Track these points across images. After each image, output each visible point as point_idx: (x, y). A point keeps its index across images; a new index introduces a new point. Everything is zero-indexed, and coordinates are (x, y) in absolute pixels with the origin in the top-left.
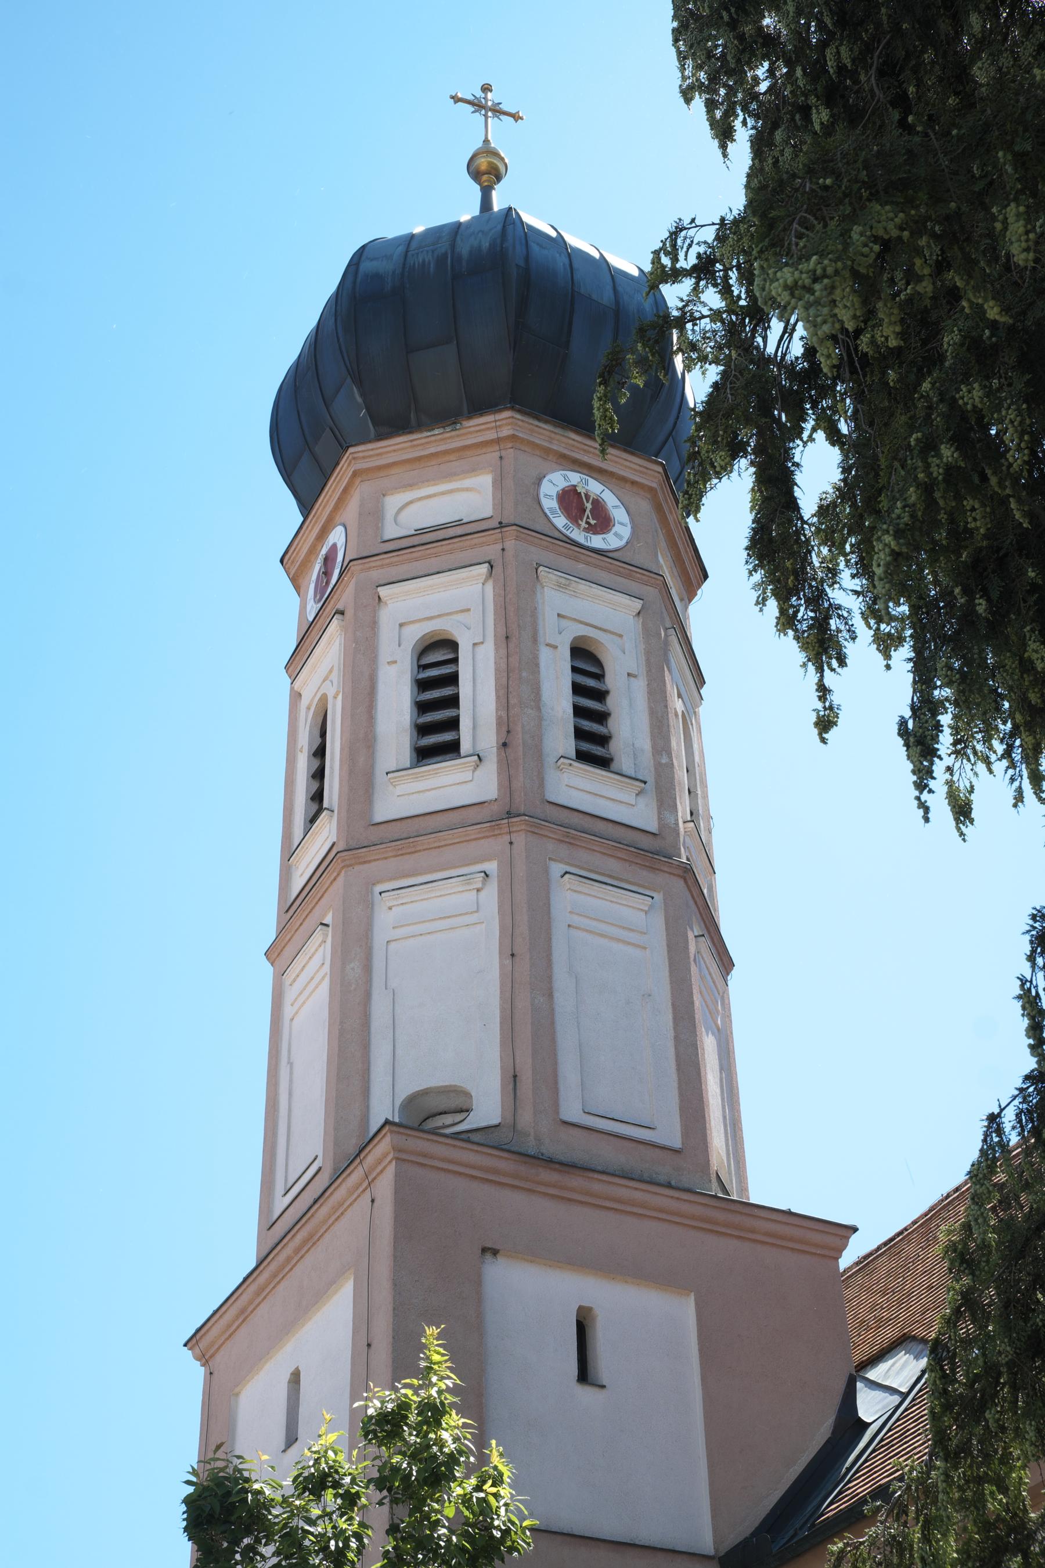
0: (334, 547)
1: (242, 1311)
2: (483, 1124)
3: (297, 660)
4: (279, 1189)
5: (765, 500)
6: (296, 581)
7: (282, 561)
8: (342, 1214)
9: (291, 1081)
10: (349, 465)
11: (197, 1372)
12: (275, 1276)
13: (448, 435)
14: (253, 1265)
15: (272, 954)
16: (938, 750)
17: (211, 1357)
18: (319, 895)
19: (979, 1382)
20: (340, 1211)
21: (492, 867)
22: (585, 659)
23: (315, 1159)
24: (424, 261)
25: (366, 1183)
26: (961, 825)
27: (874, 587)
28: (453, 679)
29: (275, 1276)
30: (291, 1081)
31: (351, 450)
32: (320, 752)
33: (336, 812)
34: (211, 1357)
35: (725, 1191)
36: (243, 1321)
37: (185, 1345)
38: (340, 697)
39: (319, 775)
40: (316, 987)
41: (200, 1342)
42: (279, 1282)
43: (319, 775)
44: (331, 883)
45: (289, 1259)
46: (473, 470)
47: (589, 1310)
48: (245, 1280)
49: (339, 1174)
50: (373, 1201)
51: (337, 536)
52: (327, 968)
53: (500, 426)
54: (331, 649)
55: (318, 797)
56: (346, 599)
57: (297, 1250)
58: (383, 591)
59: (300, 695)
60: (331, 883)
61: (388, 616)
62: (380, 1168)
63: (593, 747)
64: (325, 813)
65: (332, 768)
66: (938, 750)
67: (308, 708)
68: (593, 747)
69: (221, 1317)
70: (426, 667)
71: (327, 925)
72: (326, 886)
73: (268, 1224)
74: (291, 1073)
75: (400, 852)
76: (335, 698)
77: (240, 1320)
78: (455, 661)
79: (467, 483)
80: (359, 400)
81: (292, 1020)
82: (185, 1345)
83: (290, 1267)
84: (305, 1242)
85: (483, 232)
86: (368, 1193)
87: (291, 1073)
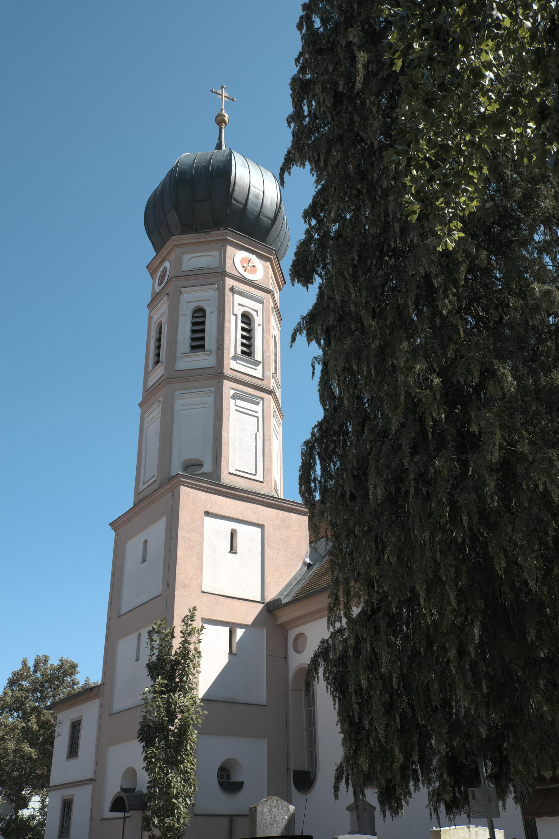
0: (165, 268)
1: (129, 518)
2: (206, 472)
3: (152, 305)
4: (142, 482)
5: (311, 523)
6: (152, 274)
11: (113, 533)
12: (140, 510)
21: (213, 389)
22: (247, 318)
28: (203, 323)
29: (140, 510)
31: (174, 237)
32: (159, 340)
43: (158, 347)
45: (145, 506)
46: (214, 250)
48: (130, 509)
49: (161, 485)
51: (167, 264)
52: (159, 415)
54: (163, 307)
55: (158, 355)
56: (170, 289)
57: (148, 504)
58: (182, 290)
59: (152, 318)
63: (198, 343)
66: (498, 816)
67: (155, 323)
68: (198, 343)
70: (195, 317)
73: (137, 493)
78: (204, 316)
79: (211, 253)
80: (177, 217)
84: (150, 502)
86: (171, 493)
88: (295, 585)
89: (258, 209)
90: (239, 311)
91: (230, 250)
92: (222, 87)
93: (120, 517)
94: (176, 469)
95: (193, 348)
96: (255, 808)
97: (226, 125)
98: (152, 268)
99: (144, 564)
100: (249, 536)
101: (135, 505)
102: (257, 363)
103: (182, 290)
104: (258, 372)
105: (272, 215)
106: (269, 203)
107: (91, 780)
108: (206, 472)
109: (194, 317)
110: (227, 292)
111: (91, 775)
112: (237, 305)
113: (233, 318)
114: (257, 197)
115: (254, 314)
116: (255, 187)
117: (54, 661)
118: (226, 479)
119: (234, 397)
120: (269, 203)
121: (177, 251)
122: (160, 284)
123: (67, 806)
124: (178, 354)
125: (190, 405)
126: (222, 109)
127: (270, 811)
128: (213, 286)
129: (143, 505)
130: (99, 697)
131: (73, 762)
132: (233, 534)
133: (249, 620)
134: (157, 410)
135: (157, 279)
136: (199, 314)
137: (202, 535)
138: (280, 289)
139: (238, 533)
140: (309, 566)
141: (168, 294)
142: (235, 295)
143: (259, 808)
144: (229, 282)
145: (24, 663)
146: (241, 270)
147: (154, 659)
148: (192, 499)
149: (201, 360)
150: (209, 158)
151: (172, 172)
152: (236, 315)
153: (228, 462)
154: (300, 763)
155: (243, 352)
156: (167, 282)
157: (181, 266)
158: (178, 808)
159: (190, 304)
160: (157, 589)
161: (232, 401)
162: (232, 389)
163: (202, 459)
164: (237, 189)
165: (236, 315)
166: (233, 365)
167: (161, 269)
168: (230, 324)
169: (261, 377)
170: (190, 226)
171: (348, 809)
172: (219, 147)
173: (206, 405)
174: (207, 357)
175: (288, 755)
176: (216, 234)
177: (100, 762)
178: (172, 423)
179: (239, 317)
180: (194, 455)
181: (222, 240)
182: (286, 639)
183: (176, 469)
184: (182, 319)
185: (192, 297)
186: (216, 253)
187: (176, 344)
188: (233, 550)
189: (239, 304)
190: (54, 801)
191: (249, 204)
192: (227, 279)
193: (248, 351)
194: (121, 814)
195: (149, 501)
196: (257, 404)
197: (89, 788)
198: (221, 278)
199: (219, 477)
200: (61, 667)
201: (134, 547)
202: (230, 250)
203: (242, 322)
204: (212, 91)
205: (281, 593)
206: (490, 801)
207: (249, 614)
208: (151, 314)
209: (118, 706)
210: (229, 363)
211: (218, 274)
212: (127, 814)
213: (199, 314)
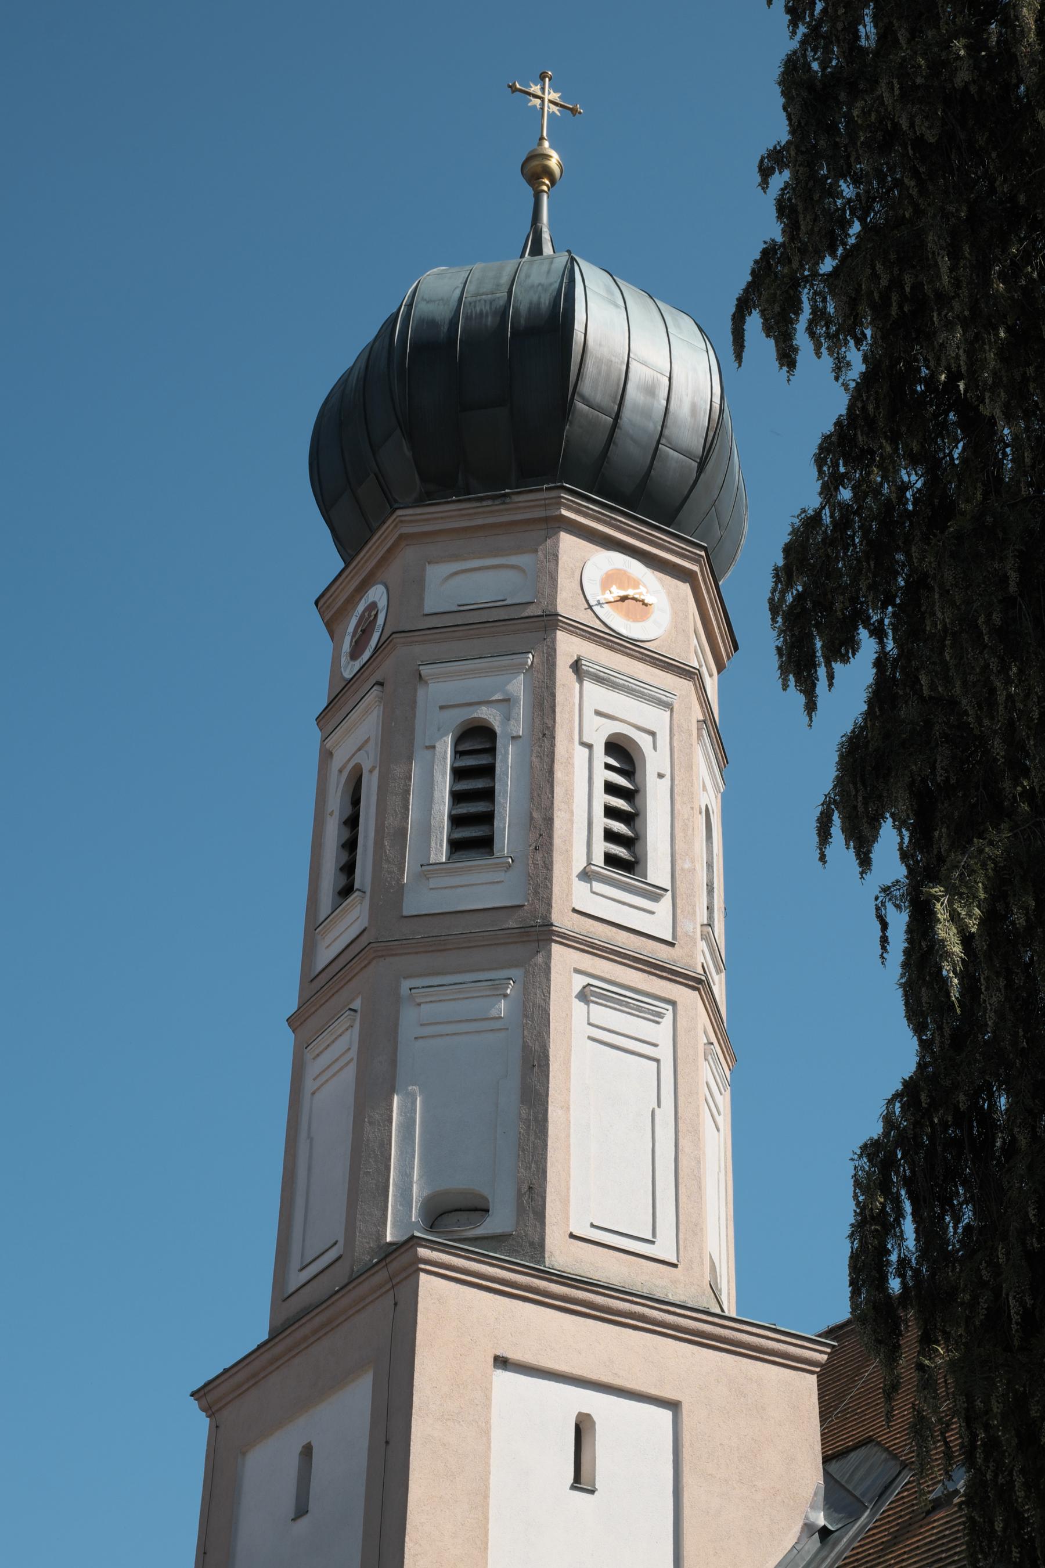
0: (373, 606)
4: (295, 1263)
6: (331, 625)
7: (317, 603)
8: (363, 1308)
9: (310, 1157)
10: (396, 526)
11: (202, 1423)
13: (496, 508)
14: (266, 1337)
15: (295, 1022)
17: (218, 1411)
18: (348, 978)
20: (362, 1304)
22: (622, 753)
23: (335, 1243)
24: (481, 311)
25: (389, 1285)
30: (310, 1157)
31: (399, 512)
32: (352, 822)
33: (368, 894)
34: (218, 1411)
35: (723, 1310)
36: (253, 1385)
37: (192, 1395)
38: (376, 772)
39: (350, 845)
40: (341, 1069)
41: (205, 1395)
42: (294, 1356)
43: (350, 845)
44: (362, 969)
45: (305, 1338)
47: (588, 1416)
48: (259, 1347)
50: (396, 1304)
51: (377, 594)
52: (353, 1053)
53: (549, 504)
54: (366, 723)
55: (349, 869)
56: (385, 669)
57: (315, 1332)
59: (331, 754)
60: (362, 969)
62: (404, 1275)
63: (473, 831)
64: (357, 894)
65: (365, 846)
67: (340, 771)
68: (473, 831)
69: (230, 1377)
71: (355, 1011)
72: (356, 971)
73: (281, 1296)
74: (311, 1148)
75: (431, 949)
76: (371, 771)
77: (251, 1383)
78: (492, 750)
79: (513, 560)
80: (408, 454)
81: (313, 1094)
82: (192, 1395)
83: (305, 1345)
85: (542, 285)
87: (311, 1148)
90: (599, 733)
92: (543, 77)
93: (226, 1371)
100: (631, 1436)
101: (275, 1334)
102: (654, 894)
103: (425, 670)
104: (658, 919)
105: (696, 444)
108: (493, 1219)
110: (563, 673)
112: (588, 714)
115: (644, 741)
118: (560, 1253)
121: (409, 554)
122: (354, 655)
125: (442, 1016)
128: (517, 659)
132: (583, 1430)
135: (347, 640)
136: (477, 743)
137: (485, 1432)
138: (720, 667)
141: (381, 684)
142: (587, 684)
148: (454, 1316)
149: (481, 887)
152: (590, 747)
153: (566, 1202)
155: (611, 860)
156: (376, 650)
161: (579, 1007)
162: (577, 971)
163: (485, 1192)
165: (590, 747)
166: (579, 895)
167: (361, 607)
168: (570, 773)
176: (526, 503)
179: (600, 749)
181: (546, 520)
188: (581, 1480)
189: (598, 713)
191: (627, 414)
193: (625, 857)
195: (318, 1321)
196: (656, 1017)
199: (538, 1247)
201: (268, 1469)
208: (329, 743)
210: (569, 894)
213: (477, 743)
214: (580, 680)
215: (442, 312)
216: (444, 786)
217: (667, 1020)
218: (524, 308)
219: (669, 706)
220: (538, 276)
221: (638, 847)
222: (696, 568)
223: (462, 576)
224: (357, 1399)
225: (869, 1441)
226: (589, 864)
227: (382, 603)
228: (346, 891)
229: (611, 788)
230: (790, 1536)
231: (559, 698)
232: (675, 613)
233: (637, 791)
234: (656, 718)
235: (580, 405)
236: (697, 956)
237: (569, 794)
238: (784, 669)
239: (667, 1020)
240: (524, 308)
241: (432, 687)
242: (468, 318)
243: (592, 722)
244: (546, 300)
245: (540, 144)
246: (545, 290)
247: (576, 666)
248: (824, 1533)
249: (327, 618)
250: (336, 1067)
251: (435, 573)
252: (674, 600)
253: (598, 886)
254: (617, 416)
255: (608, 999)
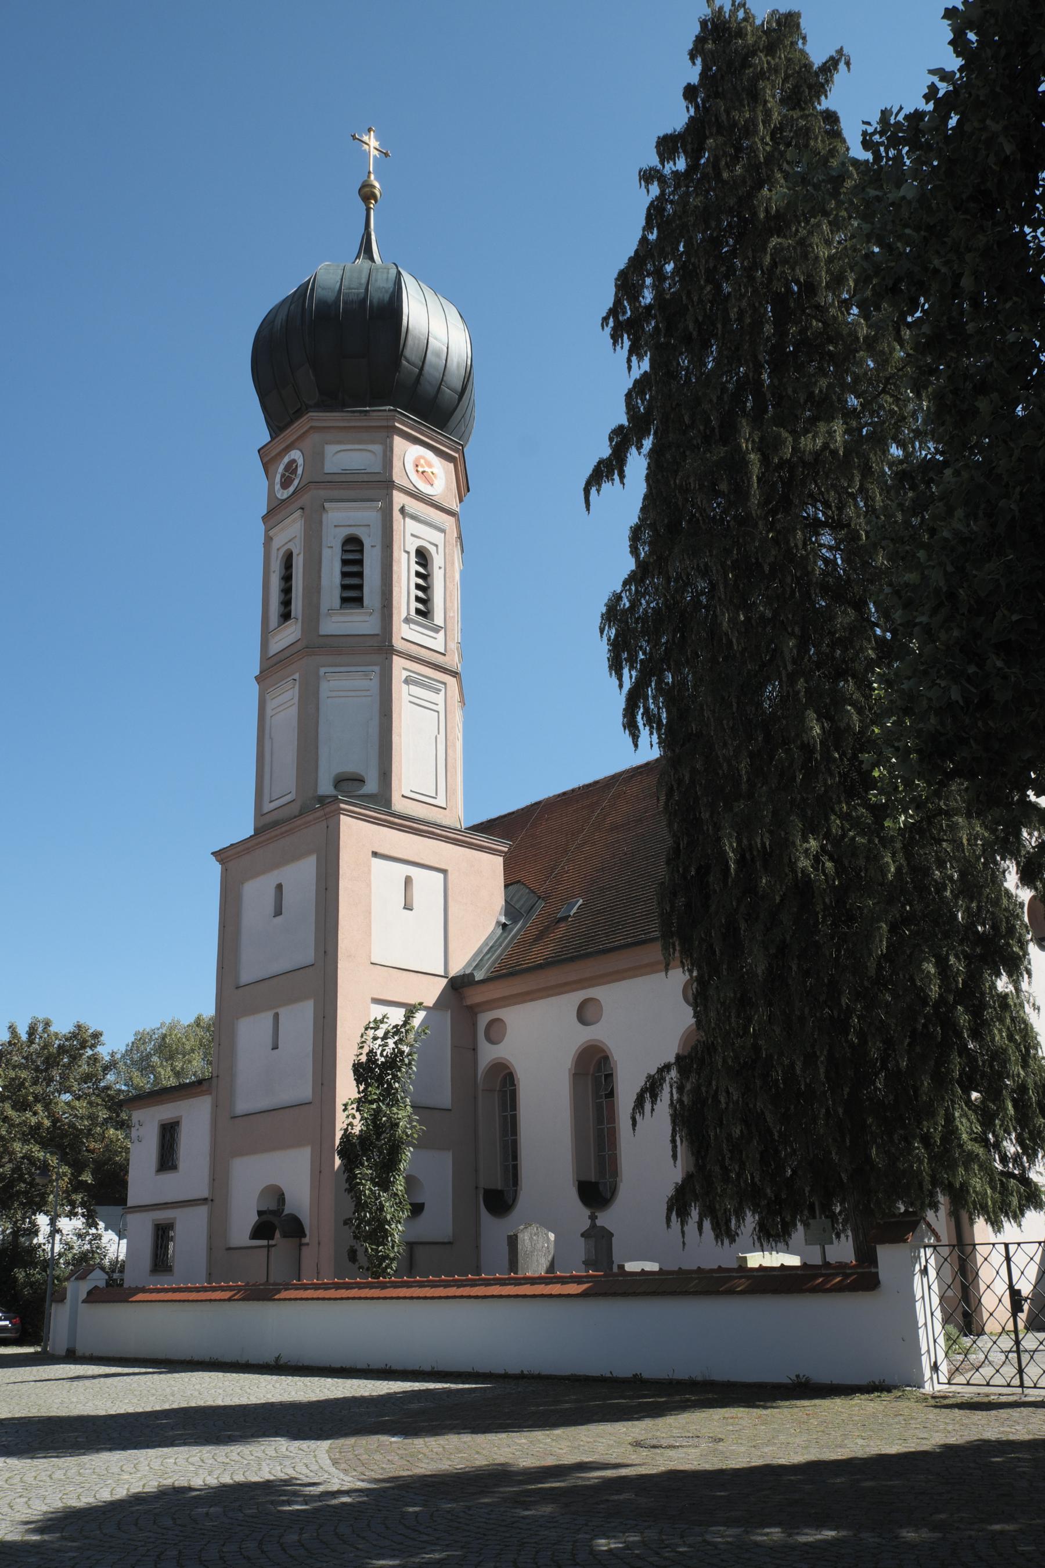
4: (266, 798)
6: (267, 466)
11: (217, 867)
14: (252, 833)
15: (265, 518)
16: (832, 1243)
19: (983, 864)
21: (377, 669)
22: (423, 556)
26: (634, 358)
27: (1007, 918)
33: (300, 620)
38: (301, 556)
39: (287, 591)
45: (276, 836)
51: (295, 454)
55: (286, 603)
56: (305, 499)
57: (282, 834)
58: (327, 505)
59: (272, 539)
61: (285, 496)
63: (352, 595)
66: (832, 1243)
68: (352, 595)
73: (259, 813)
78: (361, 551)
79: (370, 447)
80: (312, 378)
84: (286, 831)
86: (324, 823)
88: (487, 953)
89: (439, 375)
90: (412, 546)
91: (398, 441)
92: (370, 130)
94: (326, 787)
95: (344, 600)
96: (516, 1236)
97: (376, 202)
98: (268, 458)
99: (278, 918)
100: (428, 884)
101: (258, 831)
102: (436, 629)
103: (327, 505)
104: (437, 642)
105: (459, 386)
106: (455, 361)
107: (206, 1199)
108: (368, 789)
109: (344, 551)
110: (396, 514)
111: (204, 1193)
112: (409, 535)
113: (405, 556)
114: (438, 355)
115: (432, 549)
116: (436, 339)
117: (62, 1026)
118: (398, 804)
119: (407, 681)
120: (455, 364)
121: (315, 437)
122: (285, 485)
123: (163, 1233)
124: (324, 608)
125: (342, 689)
126: (369, 172)
127: (531, 1239)
128: (374, 504)
129: (273, 834)
130: (210, 1094)
131: (168, 1177)
132: (408, 881)
133: (430, 1001)
134: (290, 692)
136: (353, 545)
137: (369, 885)
139: (414, 882)
140: (504, 926)
141: (303, 509)
142: (407, 520)
143: (520, 1236)
144: (399, 499)
145: (12, 1029)
146: (414, 477)
147: (364, 1059)
148: (355, 834)
149: (359, 623)
150: (364, 281)
151: (303, 293)
152: (408, 553)
153: (400, 780)
154: (498, 1183)
155: (418, 612)
157: (323, 468)
158: (392, 1235)
159: (338, 530)
160: (307, 955)
161: (405, 687)
162: (404, 669)
163: (363, 774)
164: (410, 341)
165: (408, 553)
166: (406, 632)
168: (400, 567)
169: (443, 651)
170: (334, 398)
171: (582, 1235)
172: (366, 249)
173: (368, 693)
174: (367, 618)
175: (476, 1171)
177: (219, 1176)
178: (318, 717)
180: (351, 767)
181: (387, 427)
182: (474, 1025)
183: (326, 787)
184: (326, 553)
185: (342, 518)
186: (377, 448)
187: (319, 592)
188: (408, 907)
189: (412, 535)
190: (143, 1225)
191: (426, 368)
192: (395, 493)
193: (425, 611)
194: (264, 1242)
195: (284, 829)
196: (437, 691)
197: (203, 1210)
198: (385, 491)
199: (388, 803)
200: (74, 1036)
201: (257, 892)
202: (398, 441)
203: (417, 563)
204: (354, 136)
205: (469, 964)
206: (824, 1230)
207: (431, 992)
208: (271, 533)
209: (242, 1106)
210: (400, 630)
211: (380, 485)
212: (271, 1242)
213: (353, 545)
214: (404, 518)
215: (331, 296)
216: (337, 567)
217: (442, 693)
218: (375, 301)
219: (443, 531)
220: (382, 283)
221: (429, 604)
222: (457, 455)
223: (342, 453)
224: (306, 869)
225: (519, 882)
226: (409, 614)
227: (300, 461)
228: (286, 616)
229: (418, 574)
230: (491, 926)
231: (395, 527)
232: (447, 480)
233: (428, 575)
234: (437, 537)
235: (404, 362)
236: (453, 661)
237: (399, 578)
238: (610, 667)
239: (442, 693)
240: (375, 301)
241: (330, 514)
242: (345, 303)
243: (409, 539)
244: (387, 297)
245: (369, 177)
246: (387, 292)
247: (402, 510)
248: (504, 926)
249: (266, 460)
250: (286, 706)
251: (330, 449)
252: (446, 472)
253: (412, 626)
254: (422, 369)
255: (416, 683)
